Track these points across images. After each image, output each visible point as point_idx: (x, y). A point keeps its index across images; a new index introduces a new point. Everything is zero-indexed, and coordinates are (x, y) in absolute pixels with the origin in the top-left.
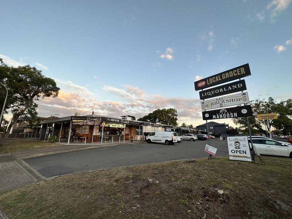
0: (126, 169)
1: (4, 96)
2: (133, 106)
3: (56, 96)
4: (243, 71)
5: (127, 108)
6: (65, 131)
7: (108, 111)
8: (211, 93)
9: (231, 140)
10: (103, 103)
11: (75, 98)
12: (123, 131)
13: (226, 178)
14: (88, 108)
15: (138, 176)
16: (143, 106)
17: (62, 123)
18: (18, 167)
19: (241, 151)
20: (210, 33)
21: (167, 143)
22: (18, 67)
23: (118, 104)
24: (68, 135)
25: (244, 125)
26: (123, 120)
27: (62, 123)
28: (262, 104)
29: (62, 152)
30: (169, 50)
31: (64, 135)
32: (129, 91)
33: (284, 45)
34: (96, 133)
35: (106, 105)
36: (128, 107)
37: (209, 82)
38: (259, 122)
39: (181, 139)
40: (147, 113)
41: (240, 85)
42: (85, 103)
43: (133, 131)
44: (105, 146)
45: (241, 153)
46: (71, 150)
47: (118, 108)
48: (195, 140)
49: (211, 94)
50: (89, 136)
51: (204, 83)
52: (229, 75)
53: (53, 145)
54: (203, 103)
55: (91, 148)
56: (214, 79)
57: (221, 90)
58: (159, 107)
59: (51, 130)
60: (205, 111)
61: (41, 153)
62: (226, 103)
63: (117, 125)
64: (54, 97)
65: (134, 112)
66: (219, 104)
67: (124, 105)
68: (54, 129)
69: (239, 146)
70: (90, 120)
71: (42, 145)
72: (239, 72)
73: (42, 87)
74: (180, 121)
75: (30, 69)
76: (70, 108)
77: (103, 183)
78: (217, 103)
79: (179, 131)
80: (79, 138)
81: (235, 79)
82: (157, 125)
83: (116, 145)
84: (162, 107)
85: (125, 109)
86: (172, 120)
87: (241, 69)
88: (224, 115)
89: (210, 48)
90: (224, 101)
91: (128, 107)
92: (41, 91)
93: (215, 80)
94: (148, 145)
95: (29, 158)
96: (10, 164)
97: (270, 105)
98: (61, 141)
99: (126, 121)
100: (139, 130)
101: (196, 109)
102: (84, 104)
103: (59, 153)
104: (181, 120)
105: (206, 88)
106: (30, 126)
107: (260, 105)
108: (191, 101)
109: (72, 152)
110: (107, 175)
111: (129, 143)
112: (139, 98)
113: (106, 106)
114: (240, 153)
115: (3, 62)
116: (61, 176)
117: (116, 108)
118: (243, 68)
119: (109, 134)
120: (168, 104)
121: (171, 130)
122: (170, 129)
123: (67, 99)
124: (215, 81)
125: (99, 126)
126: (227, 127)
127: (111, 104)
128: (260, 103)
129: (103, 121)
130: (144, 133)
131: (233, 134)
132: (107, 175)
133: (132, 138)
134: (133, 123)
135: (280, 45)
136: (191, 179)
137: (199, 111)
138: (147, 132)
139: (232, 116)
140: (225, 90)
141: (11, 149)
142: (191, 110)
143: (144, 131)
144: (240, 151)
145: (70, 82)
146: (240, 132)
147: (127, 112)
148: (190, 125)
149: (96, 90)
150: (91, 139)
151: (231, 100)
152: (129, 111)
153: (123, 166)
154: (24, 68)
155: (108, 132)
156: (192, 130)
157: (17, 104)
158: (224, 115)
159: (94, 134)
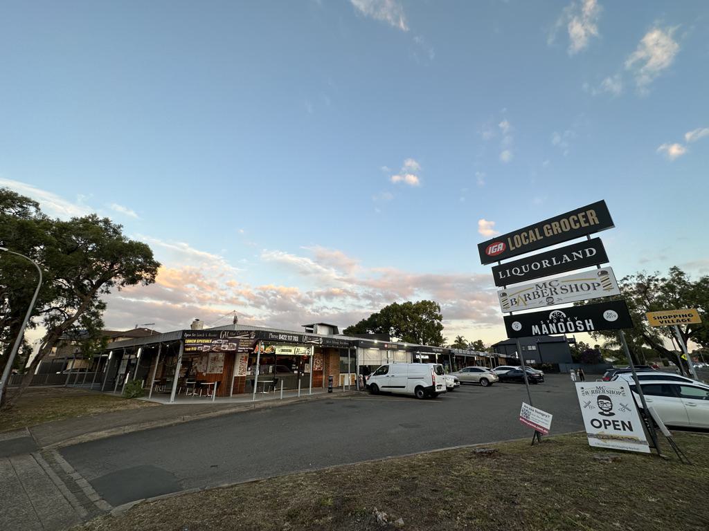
0: (315, 479)
1: (32, 289)
2: (330, 296)
3: (150, 282)
4: (593, 218)
5: (315, 302)
6: (164, 366)
7: (270, 310)
8: (521, 269)
9: (587, 391)
10: (257, 291)
11: (192, 282)
12: (308, 363)
13: (586, 510)
14: (223, 303)
15: (349, 500)
16: (355, 296)
17: (160, 347)
18: (43, 473)
19: (618, 421)
20: (501, 125)
21: (420, 393)
22: (71, 220)
23: (296, 293)
24: (174, 376)
25: (614, 340)
26: (308, 336)
27: (160, 347)
28: (655, 285)
29: (155, 424)
30: (411, 163)
31: (162, 376)
32: (319, 259)
33: (681, 141)
34: (241, 370)
35: (265, 295)
36: (319, 299)
37: (514, 245)
38: (655, 332)
39: (456, 381)
40: (366, 313)
41: (591, 252)
42: (215, 293)
43: (332, 362)
44: (263, 405)
45: (617, 427)
46: (178, 421)
47: (293, 301)
48: (492, 383)
49: (522, 272)
50: (224, 380)
51: (501, 247)
52: (560, 227)
53: (134, 405)
54: (504, 294)
55: (227, 411)
56: (526, 238)
57: (546, 264)
58: (395, 297)
59: (132, 362)
60: (511, 315)
61: (105, 429)
62: (560, 296)
63: (293, 349)
64: (147, 284)
65: (334, 310)
66: (544, 296)
67: (307, 293)
68: (140, 362)
69: (611, 409)
70: (226, 339)
71: (107, 407)
72: (584, 219)
73: (121, 263)
74: (448, 332)
75: (97, 222)
76: (179, 306)
77: (256, 524)
78: (539, 296)
79: (449, 360)
80: (198, 386)
81: (578, 235)
82: (393, 346)
83: (290, 401)
84: (404, 297)
85: (311, 303)
86: (429, 329)
87: (588, 212)
88: (559, 324)
89: (506, 156)
90: (555, 289)
91: (319, 299)
92: (117, 273)
93: (527, 240)
94: (372, 401)
95: (72, 446)
96: (25, 464)
97: (675, 287)
98: (154, 394)
99: (316, 337)
100: (347, 360)
101: (488, 300)
102: (214, 295)
103: (147, 430)
104: (451, 329)
105: (510, 257)
106: (84, 355)
107: (649, 287)
108: (473, 279)
109: (180, 424)
110: (266, 498)
111: (324, 397)
112: (346, 277)
113: (265, 298)
114: (615, 429)
115: (39, 209)
116: (150, 500)
117: (289, 302)
118: (593, 212)
119: (273, 372)
120: (416, 289)
121: (427, 357)
122: (427, 355)
123: (174, 282)
124: (527, 243)
125: (250, 354)
126: (571, 345)
127: (278, 292)
128: (650, 280)
129: (260, 340)
130: (360, 366)
131: (591, 363)
132: (266, 498)
133: (330, 381)
134: (334, 342)
135: (673, 143)
136: (490, 513)
137: (496, 305)
138: (367, 364)
139: (580, 328)
140: (555, 263)
141: (32, 419)
142: (474, 302)
143: (360, 363)
144: (613, 421)
145: (185, 245)
146: (609, 357)
147: (318, 312)
148: (477, 340)
149: (244, 260)
150: (229, 387)
151: (569, 288)
152: (322, 309)
153: (309, 467)
154: (85, 221)
155: (271, 367)
156: (481, 354)
157: (60, 303)
158: (561, 325)
159: (237, 373)
